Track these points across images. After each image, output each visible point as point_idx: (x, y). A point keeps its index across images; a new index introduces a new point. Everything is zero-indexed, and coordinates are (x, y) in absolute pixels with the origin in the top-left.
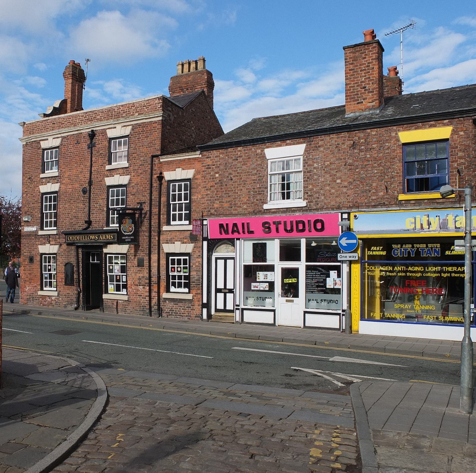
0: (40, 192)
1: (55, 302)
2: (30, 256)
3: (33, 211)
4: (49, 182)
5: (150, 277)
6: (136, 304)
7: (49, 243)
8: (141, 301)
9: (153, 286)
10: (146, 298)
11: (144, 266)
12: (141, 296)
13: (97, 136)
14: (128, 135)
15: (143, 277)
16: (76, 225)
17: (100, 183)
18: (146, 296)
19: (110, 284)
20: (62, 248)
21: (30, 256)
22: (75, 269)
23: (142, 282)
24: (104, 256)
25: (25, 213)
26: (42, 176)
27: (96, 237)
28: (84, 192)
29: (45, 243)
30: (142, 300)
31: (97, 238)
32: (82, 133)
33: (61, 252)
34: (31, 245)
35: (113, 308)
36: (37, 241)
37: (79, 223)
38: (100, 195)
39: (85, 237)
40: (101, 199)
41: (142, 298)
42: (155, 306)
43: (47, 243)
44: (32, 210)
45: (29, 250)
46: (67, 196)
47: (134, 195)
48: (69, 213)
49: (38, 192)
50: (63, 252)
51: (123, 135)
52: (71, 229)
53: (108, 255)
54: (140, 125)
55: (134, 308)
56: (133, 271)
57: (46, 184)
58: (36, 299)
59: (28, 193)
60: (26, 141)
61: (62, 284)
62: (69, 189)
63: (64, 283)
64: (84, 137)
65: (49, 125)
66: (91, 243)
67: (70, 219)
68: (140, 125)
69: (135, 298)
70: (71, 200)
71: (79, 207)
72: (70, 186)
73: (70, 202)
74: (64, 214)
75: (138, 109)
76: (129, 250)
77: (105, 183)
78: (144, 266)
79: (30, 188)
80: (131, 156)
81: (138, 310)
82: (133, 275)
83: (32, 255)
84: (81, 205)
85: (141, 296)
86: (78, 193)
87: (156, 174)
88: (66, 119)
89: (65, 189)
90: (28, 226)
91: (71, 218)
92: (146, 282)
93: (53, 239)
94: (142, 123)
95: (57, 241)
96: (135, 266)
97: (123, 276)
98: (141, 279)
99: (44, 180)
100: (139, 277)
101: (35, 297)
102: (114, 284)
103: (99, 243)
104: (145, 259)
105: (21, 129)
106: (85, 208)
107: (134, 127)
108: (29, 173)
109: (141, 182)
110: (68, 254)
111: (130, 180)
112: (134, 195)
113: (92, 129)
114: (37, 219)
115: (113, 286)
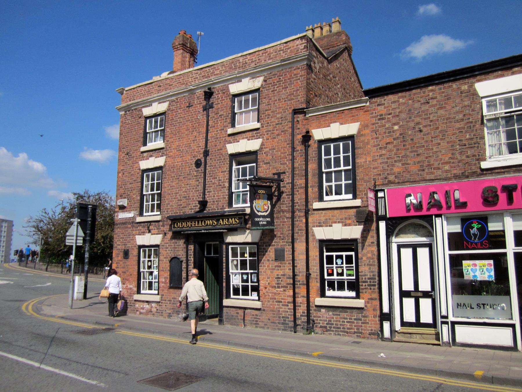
4: (151, 156)
5: (294, 275)
6: (274, 314)
7: (149, 232)
8: (281, 310)
10: (288, 306)
12: (281, 302)
13: (216, 95)
15: (284, 275)
16: (186, 207)
17: (219, 152)
20: (167, 238)
21: (128, 250)
26: (143, 149)
28: (198, 164)
30: (281, 308)
31: (216, 223)
34: (127, 235)
35: (238, 319)
36: (134, 230)
37: (190, 204)
38: (220, 167)
40: (221, 172)
41: (283, 305)
47: (269, 163)
48: (177, 193)
50: (168, 243)
55: (269, 319)
59: (125, 172)
62: (178, 162)
67: (178, 200)
71: (190, 184)
72: (180, 159)
73: (178, 178)
75: (272, 55)
76: (261, 237)
80: (263, 114)
82: (269, 272)
83: (128, 248)
84: (193, 182)
85: (281, 302)
86: (189, 167)
91: (179, 198)
92: (288, 282)
96: (271, 260)
100: (277, 275)
106: (198, 186)
108: (127, 148)
109: (278, 146)
111: (262, 144)
112: (269, 163)
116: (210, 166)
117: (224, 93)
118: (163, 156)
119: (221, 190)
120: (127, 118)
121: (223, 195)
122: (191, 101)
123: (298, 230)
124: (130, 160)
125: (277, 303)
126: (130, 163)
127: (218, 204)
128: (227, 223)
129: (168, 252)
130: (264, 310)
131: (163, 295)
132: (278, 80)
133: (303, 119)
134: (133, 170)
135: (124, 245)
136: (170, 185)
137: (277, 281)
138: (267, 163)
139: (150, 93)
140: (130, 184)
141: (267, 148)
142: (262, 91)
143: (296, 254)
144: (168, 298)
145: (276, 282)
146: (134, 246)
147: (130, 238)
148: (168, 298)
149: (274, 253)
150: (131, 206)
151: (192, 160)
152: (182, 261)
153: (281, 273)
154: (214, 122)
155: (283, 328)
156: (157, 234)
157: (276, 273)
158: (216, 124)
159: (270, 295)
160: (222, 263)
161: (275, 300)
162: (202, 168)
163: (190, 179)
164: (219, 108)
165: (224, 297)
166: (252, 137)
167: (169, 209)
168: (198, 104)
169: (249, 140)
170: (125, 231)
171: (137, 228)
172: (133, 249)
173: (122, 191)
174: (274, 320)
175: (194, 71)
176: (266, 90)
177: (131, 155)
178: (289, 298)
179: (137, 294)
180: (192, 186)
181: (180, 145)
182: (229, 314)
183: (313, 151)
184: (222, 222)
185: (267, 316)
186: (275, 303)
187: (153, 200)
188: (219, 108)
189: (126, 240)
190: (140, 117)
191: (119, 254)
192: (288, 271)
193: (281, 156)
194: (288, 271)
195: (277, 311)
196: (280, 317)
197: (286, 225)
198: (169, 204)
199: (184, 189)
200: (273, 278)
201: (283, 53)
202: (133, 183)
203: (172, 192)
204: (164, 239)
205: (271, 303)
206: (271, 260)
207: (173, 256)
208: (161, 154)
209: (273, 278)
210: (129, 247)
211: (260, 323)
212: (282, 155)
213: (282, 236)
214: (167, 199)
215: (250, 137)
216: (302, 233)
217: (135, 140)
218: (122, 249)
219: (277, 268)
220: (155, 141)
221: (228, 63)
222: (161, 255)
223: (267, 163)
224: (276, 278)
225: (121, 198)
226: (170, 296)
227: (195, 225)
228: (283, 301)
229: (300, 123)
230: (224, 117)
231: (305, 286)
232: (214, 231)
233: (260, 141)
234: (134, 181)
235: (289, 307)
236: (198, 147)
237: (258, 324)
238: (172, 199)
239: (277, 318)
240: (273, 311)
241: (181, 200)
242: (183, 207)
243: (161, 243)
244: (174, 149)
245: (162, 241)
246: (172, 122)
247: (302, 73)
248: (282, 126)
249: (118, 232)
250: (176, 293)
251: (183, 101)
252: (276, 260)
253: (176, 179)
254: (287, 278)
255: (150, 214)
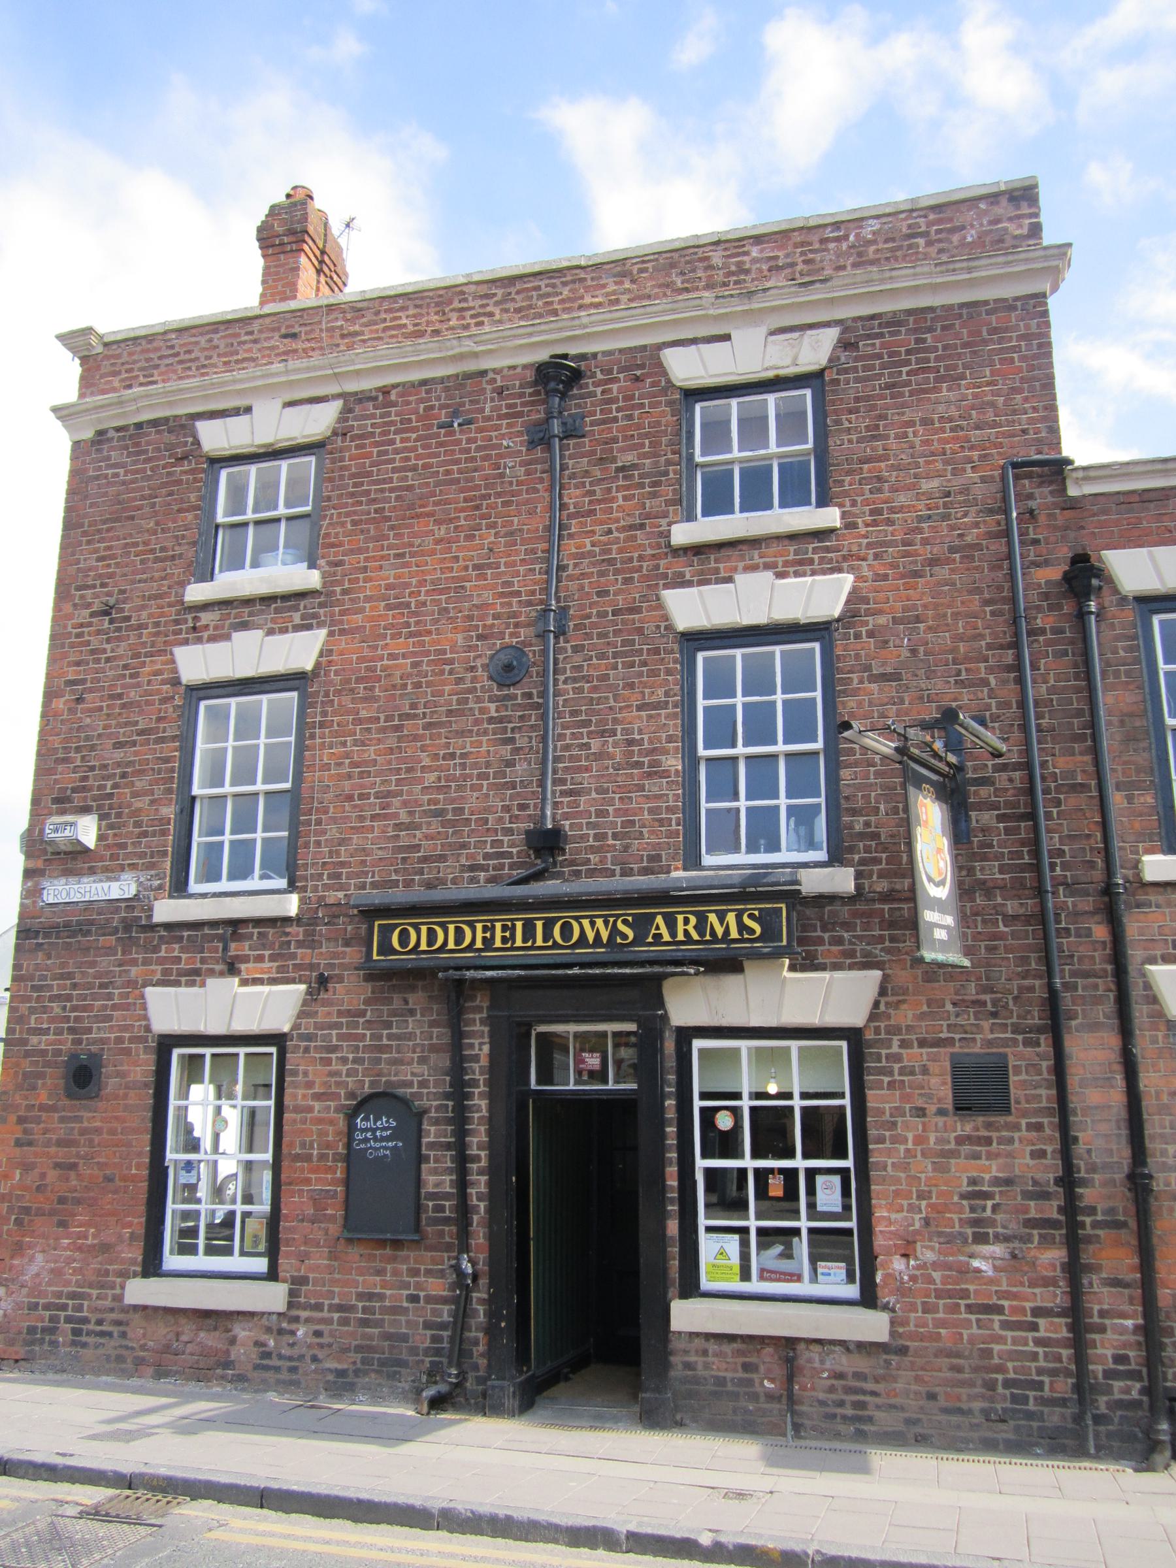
0: (176, 682)
1: (254, 1353)
2: (96, 1058)
3: (115, 786)
4: (244, 626)
5: (1069, 1180)
6: (958, 1369)
7: (232, 969)
8: (996, 1348)
9: (1089, 1240)
10: (1034, 1327)
11: (1006, 1110)
12: (999, 1310)
13: (596, 385)
14: (820, 374)
15: (1008, 1182)
16: (442, 858)
17: (624, 622)
18: (1038, 1312)
19: (709, 1229)
20: (326, 1003)
21: (96, 1058)
22: (432, 1133)
23: (999, 1217)
24: (670, 1046)
25: (57, 801)
26: (196, 592)
27: (621, 927)
29: (197, 972)
30: (1001, 1340)
31: (630, 934)
32: (483, 373)
33: (317, 1026)
34: (90, 986)
35: (754, 1397)
36: (134, 962)
37: (464, 846)
38: (631, 686)
39: (509, 928)
40: (639, 708)
41: (1006, 1325)
42: (1117, 1384)
43: (211, 973)
44: (109, 783)
45: (67, 1019)
46: (375, 699)
47: (895, 677)
48: (390, 794)
49: (163, 682)
50: (337, 1026)
51: (782, 372)
52: (408, 884)
53: (698, 1044)
54: (900, 323)
55: (932, 1396)
56: (919, 1140)
57: (227, 637)
58: (102, 1334)
59: (91, 690)
60: (99, 421)
61: (320, 1236)
62: (392, 657)
63: (335, 1229)
64: (500, 391)
65: (255, 341)
66: (582, 965)
67: (398, 827)
68: (900, 323)
69: (942, 1323)
70: (408, 717)
71: (463, 756)
72: (401, 645)
73: (398, 728)
74: (350, 798)
75: (872, 248)
76: (876, 1004)
77: (666, 618)
78: (1006, 1110)
79: (108, 660)
80: (849, 473)
81: (970, 1412)
82: (925, 1168)
84: (484, 747)
85: (999, 1310)
86: (460, 681)
87: (1047, 563)
88: (377, 313)
89: (361, 660)
90: (68, 873)
91: (404, 818)
92: (1033, 1214)
93: (264, 947)
94: (909, 312)
95: (293, 956)
96: (932, 1109)
97: (820, 1180)
98: (987, 1196)
99: (206, 618)
100: (973, 1182)
101: (93, 1318)
102: (744, 1231)
103: (642, 964)
104: (1012, 1062)
105: (73, 369)
106: (510, 764)
107: (353, 402)
108: (103, 585)
109: (936, 606)
110: (380, 1038)
111: (855, 597)
112: (895, 677)
113: (560, 350)
114: (145, 834)
115: (732, 1243)
116: (575, 680)
117: (637, 379)
118: (309, 627)
119: (641, 788)
120: (109, 458)
121: (651, 811)
122: (463, 405)
123: (1074, 974)
124: (119, 639)
125: (973, 1317)
126: (121, 651)
127: (626, 848)
128: (695, 936)
129: (335, 1067)
130: (903, 1351)
131: (298, 1282)
132: (913, 345)
133: (1055, 505)
134: (138, 685)
135: (72, 1030)
136: (347, 755)
137: (973, 1209)
138: (884, 677)
139: (237, 362)
140: (118, 745)
141: (880, 612)
142: (836, 382)
143: (1074, 1080)
144: (331, 1295)
145: (967, 1215)
146: (132, 1040)
147: (110, 997)
148: (331, 1295)
149: (949, 1079)
150: (123, 846)
151: (470, 648)
152: (421, 1114)
153: (994, 1169)
154: (592, 493)
155: (1011, 1436)
156: (273, 981)
157: (962, 1172)
158: (599, 502)
159: (937, 1275)
160: (662, 1123)
161: (962, 1302)
162: (530, 685)
163: (461, 733)
164: (615, 440)
165: (673, 1291)
166: (801, 563)
167: (342, 864)
168: (500, 417)
169: (781, 575)
170: (80, 965)
171: (156, 949)
172: (127, 1052)
173: (67, 777)
174: (959, 1399)
175: (473, 288)
176: (857, 380)
177: (128, 619)
178: (1037, 1291)
179: (146, 1274)
180: (475, 766)
181: (408, 585)
182: (701, 1372)
183: (1118, 638)
184: (664, 930)
185: (918, 1379)
186: (964, 1316)
187: (244, 823)
188: (615, 440)
189: (85, 1009)
190: (185, 457)
191: (41, 1075)
192: (1028, 1160)
193: (954, 650)
194: (1031, 1163)
195: (975, 1354)
196: (991, 1386)
197: (1008, 950)
198: (342, 842)
199: (430, 778)
200: (951, 1193)
201: (929, 243)
202: (134, 743)
203: (362, 787)
204: (314, 1008)
205: (941, 1315)
206: (932, 1109)
207: (367, 1090)
208: (297, 618)
209: (951, 1193)
210: (103, 1041)
211: (878, 1415)
212: (962, 647)
213: (987, 997)
214: (334, 820)
215: (786, 564)
216: (1095, 987)
217: (153, 551)
218: (58, 1053)
219: (966, 1148)
220: (255, 564)
221: (649, 265)
222: (295, 1085)
223: (884, 677)
224: (963, 1196)
225: (63, 812)
226: (346, 1283)
227: (513, 937)
228: (1006, 1303)
229: (1042, 519)
230: (641, 476)
231: (1129, 1237)
232: (616, 971)
233: (847, 580)
234: (141, 733)
235: (1042, 1333)
236: (502, 595)
237: (870, 1419)
238: (361, 818)
239: (978, 1390)
240: (950, 1354)
241: (412, 826)
242: (425, 859)
243: (296, 1027)
244: (368, 599)
245: (301, 1014)
246: (355, 485)
247: (1027, 327)
248: (952, 528)
249: (37, 967)
250: (380, 1272)
251: (422, 401)
252: (962, 1107)
253: (383, 730)
254: (1027, 1195)
255: (224, 885)
